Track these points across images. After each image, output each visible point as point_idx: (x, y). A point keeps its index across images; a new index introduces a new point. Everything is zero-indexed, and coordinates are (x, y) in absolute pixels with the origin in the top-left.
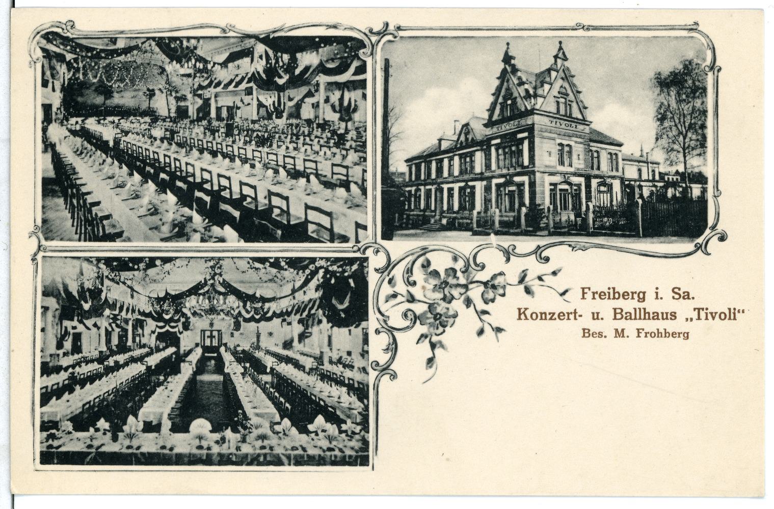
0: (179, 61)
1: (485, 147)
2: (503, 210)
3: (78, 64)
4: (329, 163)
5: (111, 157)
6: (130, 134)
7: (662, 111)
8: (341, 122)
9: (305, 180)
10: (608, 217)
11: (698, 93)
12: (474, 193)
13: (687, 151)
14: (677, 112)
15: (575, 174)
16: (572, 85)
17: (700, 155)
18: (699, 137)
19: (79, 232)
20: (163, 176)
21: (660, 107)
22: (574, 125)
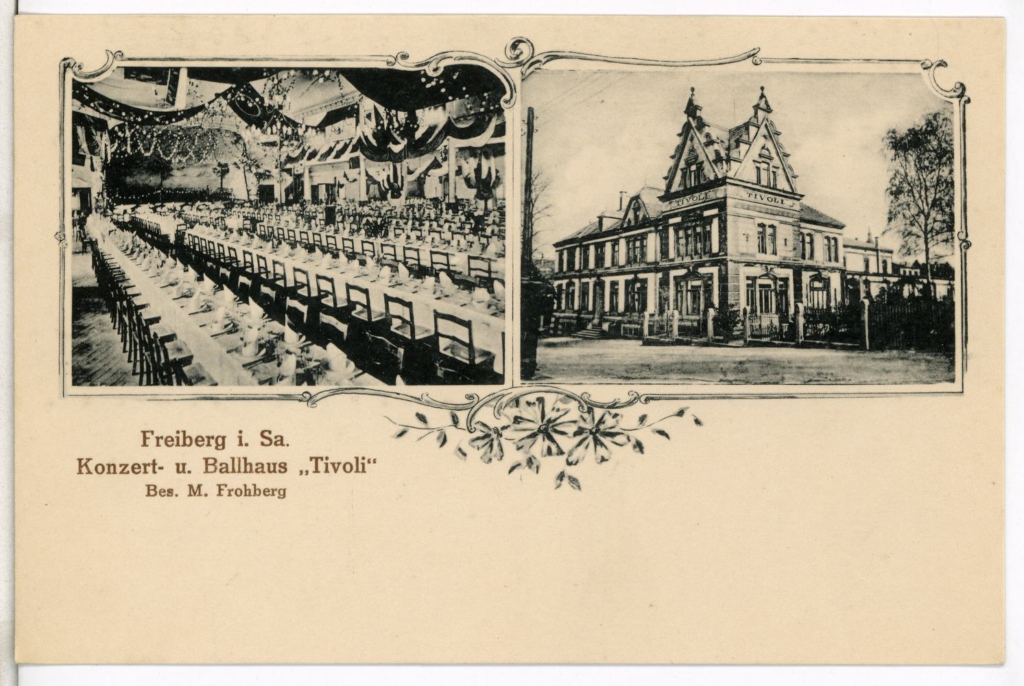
0: (259, 125)
1: (660, 228)
2: (684, 312)
3: (124, 132)
4: (464, 256)
5: (172, 256)
8: (479, 201)
9: (432, 279)
10: (824, 323)
11: (945, 159)
12: (646, 288)
13: (929, 236)
14: (917, 183)
16: (777, 146)
17: (946, 241)
18: (946, 218)
19: (132, 359)
21: (894, 178)
22: (779, 199)
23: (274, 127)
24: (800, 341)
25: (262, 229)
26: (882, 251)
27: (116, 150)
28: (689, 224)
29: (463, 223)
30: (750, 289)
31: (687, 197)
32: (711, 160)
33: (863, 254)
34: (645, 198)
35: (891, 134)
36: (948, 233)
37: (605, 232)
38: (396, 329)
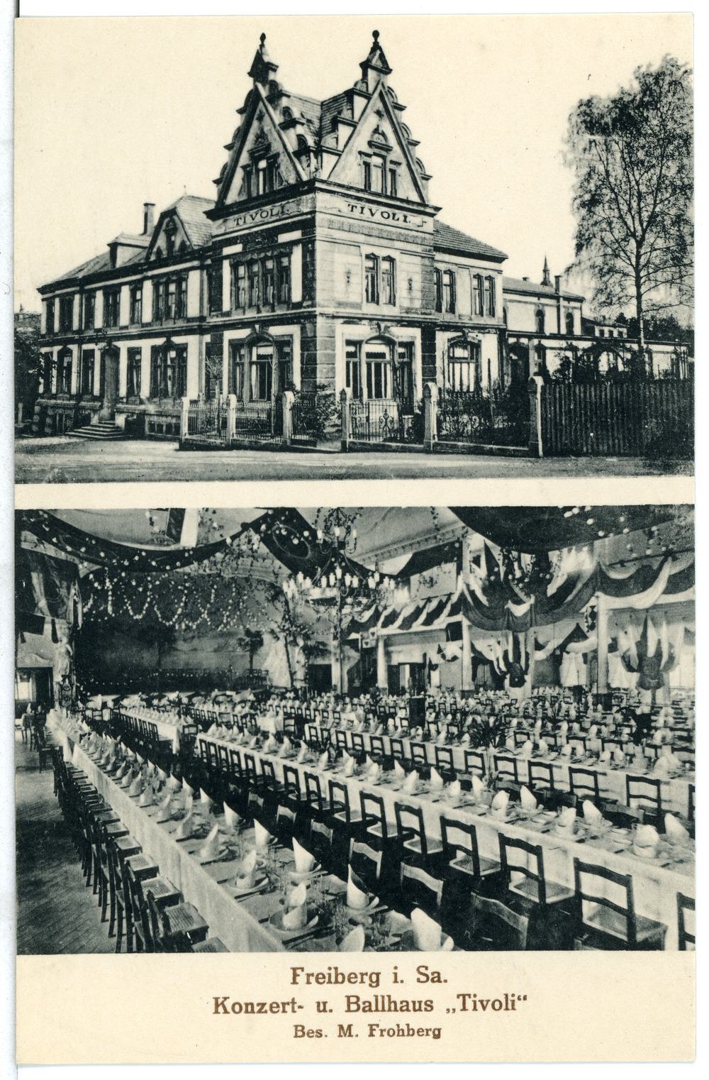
0: (310, 573)
1: (209, 262)
3: (102, 583)
4: (622, 775)
6: (213, 727)
7: (592, 187)
8: (643, 691)
9: (573, 811)
10: (469, 414)
12: (185, 360)
13: (642, 274)
15: (401, 322)
16: (400, 129)
18: (672, 243)
19: (115, 931)
20: (282, 810)
22: (400, 214)
23: (332, 577)
24: (432, 442)
25: (313, 732)
26: (568, 299)
27: (90, 610)
28: (255, 256)
29: (618, 725)
30: (352, 360)
31: (252, 212)
32: (291, 150)
33: (535, 304)
34: (185, 213)
35: (584, 108)
36: (674, 269)
37: (121, 269)
38: (517, 887)
